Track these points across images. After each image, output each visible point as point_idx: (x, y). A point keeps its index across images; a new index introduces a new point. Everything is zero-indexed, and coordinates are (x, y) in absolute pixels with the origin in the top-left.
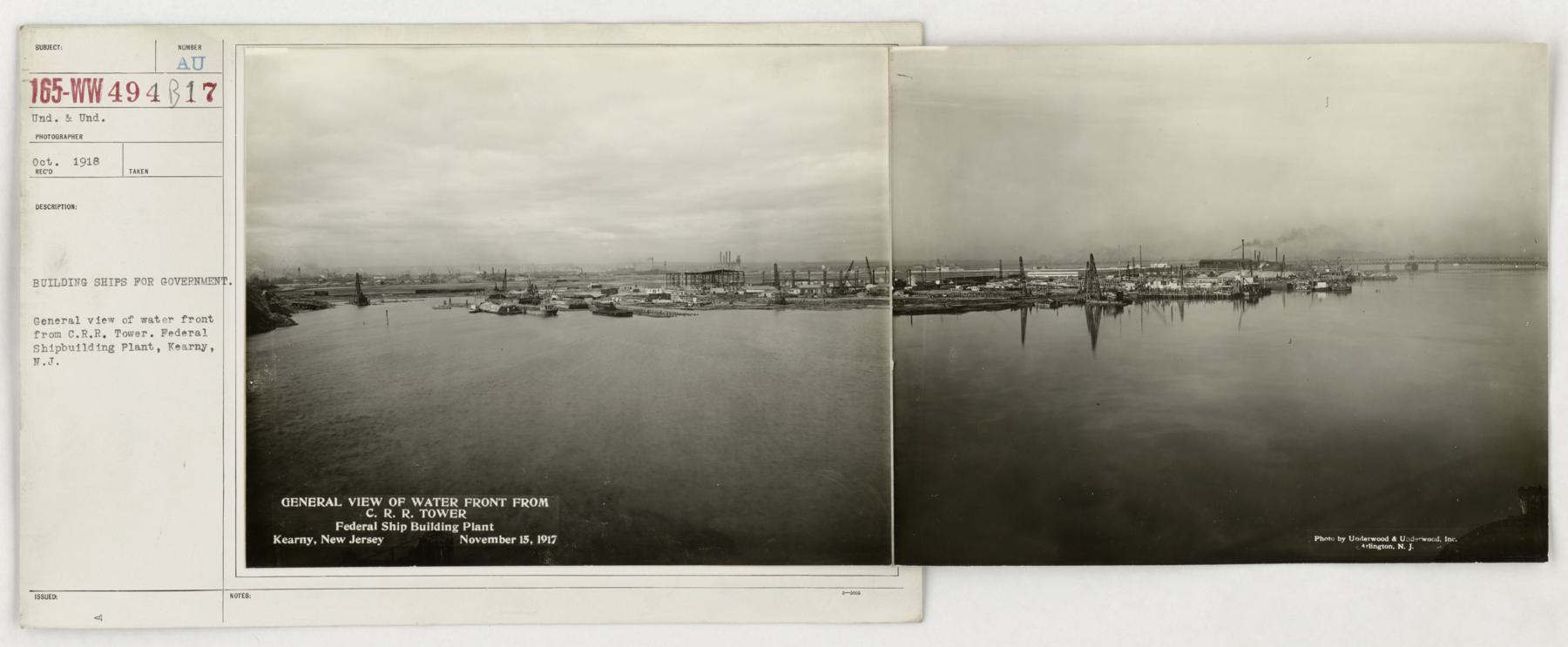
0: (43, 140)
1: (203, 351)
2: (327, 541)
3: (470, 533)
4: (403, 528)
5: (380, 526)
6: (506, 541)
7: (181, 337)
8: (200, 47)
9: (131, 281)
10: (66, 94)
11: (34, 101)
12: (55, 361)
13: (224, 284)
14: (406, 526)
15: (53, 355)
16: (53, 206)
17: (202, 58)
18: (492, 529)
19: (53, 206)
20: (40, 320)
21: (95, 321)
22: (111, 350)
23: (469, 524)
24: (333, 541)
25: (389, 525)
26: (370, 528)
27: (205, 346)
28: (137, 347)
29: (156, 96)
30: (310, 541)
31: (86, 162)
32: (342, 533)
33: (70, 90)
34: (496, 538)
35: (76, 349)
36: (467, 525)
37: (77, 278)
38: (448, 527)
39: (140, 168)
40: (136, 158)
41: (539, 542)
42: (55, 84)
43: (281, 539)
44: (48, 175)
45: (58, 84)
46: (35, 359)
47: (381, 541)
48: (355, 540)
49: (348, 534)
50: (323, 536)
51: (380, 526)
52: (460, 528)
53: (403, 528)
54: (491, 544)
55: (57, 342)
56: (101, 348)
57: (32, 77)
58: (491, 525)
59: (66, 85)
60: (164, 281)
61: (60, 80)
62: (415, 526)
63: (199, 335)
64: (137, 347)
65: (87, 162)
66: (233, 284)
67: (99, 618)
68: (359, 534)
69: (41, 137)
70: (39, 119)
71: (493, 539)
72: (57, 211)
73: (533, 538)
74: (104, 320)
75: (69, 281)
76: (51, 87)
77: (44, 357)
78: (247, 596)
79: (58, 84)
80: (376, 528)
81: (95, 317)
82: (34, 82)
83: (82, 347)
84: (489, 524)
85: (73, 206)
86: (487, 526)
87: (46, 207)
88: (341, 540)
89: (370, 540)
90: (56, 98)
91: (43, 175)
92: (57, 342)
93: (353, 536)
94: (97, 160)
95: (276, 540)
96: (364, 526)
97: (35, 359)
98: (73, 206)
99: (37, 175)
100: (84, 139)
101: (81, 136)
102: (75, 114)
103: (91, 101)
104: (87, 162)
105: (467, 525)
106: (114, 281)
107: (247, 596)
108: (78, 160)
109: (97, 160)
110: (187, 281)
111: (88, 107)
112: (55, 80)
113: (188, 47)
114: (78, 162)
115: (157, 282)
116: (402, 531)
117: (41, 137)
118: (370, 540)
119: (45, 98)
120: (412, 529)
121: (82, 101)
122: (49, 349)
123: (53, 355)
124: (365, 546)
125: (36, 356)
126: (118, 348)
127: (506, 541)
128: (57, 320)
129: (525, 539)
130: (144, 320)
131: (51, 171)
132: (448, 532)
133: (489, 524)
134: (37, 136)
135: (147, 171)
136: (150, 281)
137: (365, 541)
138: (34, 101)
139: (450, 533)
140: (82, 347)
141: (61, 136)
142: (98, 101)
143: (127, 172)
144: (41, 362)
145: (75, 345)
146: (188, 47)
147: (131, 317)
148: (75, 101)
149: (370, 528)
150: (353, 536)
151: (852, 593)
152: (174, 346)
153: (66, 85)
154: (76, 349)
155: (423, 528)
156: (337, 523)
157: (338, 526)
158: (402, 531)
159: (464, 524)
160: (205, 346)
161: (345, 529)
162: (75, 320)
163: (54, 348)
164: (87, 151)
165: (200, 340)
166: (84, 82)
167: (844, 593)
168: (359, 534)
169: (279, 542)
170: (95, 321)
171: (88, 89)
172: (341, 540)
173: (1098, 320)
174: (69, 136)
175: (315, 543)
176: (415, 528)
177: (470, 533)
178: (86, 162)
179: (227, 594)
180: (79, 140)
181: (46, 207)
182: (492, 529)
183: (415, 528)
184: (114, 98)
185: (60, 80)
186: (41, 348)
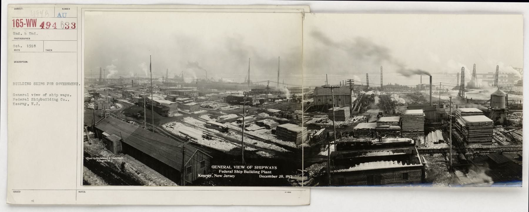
0: (17, 40)
1: (25, 105)
2: (216, 176)
3: (263, 174)
4: (241, 172)
5: (234, 172)
6: (274, 177)
7: (18, 101)
8: (69, 9)
9: (46, 84)
10: (25, 24)
11: (14, 26)
12: (38, 104)
13: (77, 85)
14: (242, 172)
15: (38, 102)
16: (20, 62)
17: (66, 13)
18: (271, 173)
19: (20, 62)
20: (15, 94)
21: (34, 95)
22: (57, 100)
23: (263, 171)
24: (218, 176)
25: (236, 171)
26: (230, 172)
27: (26, 104)
28: (19, 104)
29: (55, 27)
30: (210, 176)
31: (31, 46)
32: (221, 174)
33: (26, 23)
34: (271, 176)
35: (45, 100)
36: (263, 171)
37: (28, 82)
38: (256, 172)
39: (49, 49)
40: (48, 46)
41: (286, 177)
42: (20, 21)
43: (200, 175)
44: (18, 51)
45: (22, 21)
46: (32, 103)
47: (234, 176)
48: (225, 176)
49: (223, 174)
50: (215, 175)
51: (234, 172)
52: (260, 172)
53: (241, 172)
54: (269, 178)
55: (39, 97)
56: (54, 99)
57: (13, 19)
58: (271, 172)
59: (24, 21)
60: (57, 84)
61: (22, 19)
62: (245, 172)
63: (44, 100)
64: (19, 104)
65: (32, 46)
66: (81, 85)
67: (33, 201)
68: (227, 174)
69: (16, 39)
70: (15, 34)
71: (270, 176)
72: (21, 63)
73: (284, 176)
74: (37, 95)
75: (25, 83)
76: (19, 22)
77: (35, 102)
78: (85, 192)
79: (22, 21)
80: (232, 172)
81: (34, 94)
82: (14, 20)
83: (47, 99)
84: (270, 171)
85: (27, 62)
86: (269, 172)
87: (18, 62)
88: (221, 176)
89: (230, 176)
90: (21, 26)
91: (17, 51)
92: (39, 97)
93: (225, 175)
94: (35, 45)
95: (199, 175)
96: (228, 171)
97: (32, 103)
98: (27, 62)
99: (15, 51)
100: (31, 39)
101: (29, 39)
102: (28, 31)
103: (33, 26)
104: (32, 46)
105: (263, 171)
106: (40, 84)
107: (85, 192)
108: (29, 46)
109: (35, 45)
110: (65, 84)
111: (32, 29)
112: (21, 20)
113: (65, 9)
114: (29, 46)
115: (55, 84)
116: (241, 173)
117: (16, 39)
118: (230, 176)
119: (18, 26)
120: (244, 173)
121: (30, 27)
122: (36, 100)
123: (38, 102)
124: (229, 178)
125: (32, 102)
126: (59, 100)
127: (274, 177)
128: (21, 95)
129: (281, 176)
130: (61, 95)
131: (19, 50)
132: (256, 173)
133: (270, 171)
134: (15, 38)
135: (52, 50)
136: (43, 84)
137: (229, 176)
138: (14, 26)
139: (257, 174)
140: (47, 99)
141: (23, 38)
142: (35, 26)
143: (45, 50)
144: (34, 104)
145: (45, 99)
146: (65, 9)
147: (46, 94)
148: (28, 26)
149: (230, 172)
150: (225, 175)
151: (288, 192)
152: (15, 104)
153: (24, 21)
154: (45, 100)
155: (248, 172)
156: (220, 170)
157: (220, 171)
158: (241, 173)
159: (262, 171)
160: (26, 104)
161: (222, 172)
162: (27, 95)
163: (38, 100)
164: (33, 43)
165: (24, 102)
166: (31, 20)
167: (285, 192)
168: (227, 174)
169: (200, 176)
170: (34, 95)
171: (32, 23)
172: (221, 176)
173: (348, 106)
174: (26, 38)
175: (212, 177)
176: (245, 172)
177: (263, 174)
178: (31, 46)
179: (78, 191)
180: (29, 40)
181: (18, 62)
182: (271, 173)
183: (245, 172)
184: (41, 27)
185: (22, 19)
186: (34, 99)
